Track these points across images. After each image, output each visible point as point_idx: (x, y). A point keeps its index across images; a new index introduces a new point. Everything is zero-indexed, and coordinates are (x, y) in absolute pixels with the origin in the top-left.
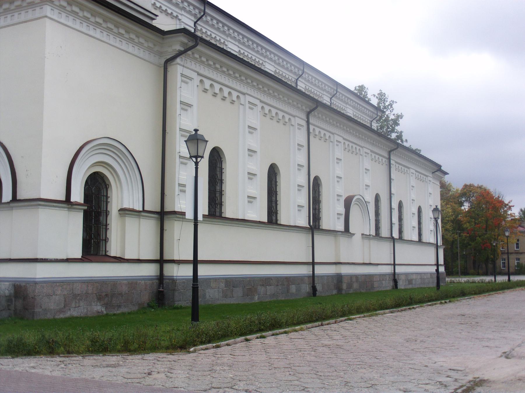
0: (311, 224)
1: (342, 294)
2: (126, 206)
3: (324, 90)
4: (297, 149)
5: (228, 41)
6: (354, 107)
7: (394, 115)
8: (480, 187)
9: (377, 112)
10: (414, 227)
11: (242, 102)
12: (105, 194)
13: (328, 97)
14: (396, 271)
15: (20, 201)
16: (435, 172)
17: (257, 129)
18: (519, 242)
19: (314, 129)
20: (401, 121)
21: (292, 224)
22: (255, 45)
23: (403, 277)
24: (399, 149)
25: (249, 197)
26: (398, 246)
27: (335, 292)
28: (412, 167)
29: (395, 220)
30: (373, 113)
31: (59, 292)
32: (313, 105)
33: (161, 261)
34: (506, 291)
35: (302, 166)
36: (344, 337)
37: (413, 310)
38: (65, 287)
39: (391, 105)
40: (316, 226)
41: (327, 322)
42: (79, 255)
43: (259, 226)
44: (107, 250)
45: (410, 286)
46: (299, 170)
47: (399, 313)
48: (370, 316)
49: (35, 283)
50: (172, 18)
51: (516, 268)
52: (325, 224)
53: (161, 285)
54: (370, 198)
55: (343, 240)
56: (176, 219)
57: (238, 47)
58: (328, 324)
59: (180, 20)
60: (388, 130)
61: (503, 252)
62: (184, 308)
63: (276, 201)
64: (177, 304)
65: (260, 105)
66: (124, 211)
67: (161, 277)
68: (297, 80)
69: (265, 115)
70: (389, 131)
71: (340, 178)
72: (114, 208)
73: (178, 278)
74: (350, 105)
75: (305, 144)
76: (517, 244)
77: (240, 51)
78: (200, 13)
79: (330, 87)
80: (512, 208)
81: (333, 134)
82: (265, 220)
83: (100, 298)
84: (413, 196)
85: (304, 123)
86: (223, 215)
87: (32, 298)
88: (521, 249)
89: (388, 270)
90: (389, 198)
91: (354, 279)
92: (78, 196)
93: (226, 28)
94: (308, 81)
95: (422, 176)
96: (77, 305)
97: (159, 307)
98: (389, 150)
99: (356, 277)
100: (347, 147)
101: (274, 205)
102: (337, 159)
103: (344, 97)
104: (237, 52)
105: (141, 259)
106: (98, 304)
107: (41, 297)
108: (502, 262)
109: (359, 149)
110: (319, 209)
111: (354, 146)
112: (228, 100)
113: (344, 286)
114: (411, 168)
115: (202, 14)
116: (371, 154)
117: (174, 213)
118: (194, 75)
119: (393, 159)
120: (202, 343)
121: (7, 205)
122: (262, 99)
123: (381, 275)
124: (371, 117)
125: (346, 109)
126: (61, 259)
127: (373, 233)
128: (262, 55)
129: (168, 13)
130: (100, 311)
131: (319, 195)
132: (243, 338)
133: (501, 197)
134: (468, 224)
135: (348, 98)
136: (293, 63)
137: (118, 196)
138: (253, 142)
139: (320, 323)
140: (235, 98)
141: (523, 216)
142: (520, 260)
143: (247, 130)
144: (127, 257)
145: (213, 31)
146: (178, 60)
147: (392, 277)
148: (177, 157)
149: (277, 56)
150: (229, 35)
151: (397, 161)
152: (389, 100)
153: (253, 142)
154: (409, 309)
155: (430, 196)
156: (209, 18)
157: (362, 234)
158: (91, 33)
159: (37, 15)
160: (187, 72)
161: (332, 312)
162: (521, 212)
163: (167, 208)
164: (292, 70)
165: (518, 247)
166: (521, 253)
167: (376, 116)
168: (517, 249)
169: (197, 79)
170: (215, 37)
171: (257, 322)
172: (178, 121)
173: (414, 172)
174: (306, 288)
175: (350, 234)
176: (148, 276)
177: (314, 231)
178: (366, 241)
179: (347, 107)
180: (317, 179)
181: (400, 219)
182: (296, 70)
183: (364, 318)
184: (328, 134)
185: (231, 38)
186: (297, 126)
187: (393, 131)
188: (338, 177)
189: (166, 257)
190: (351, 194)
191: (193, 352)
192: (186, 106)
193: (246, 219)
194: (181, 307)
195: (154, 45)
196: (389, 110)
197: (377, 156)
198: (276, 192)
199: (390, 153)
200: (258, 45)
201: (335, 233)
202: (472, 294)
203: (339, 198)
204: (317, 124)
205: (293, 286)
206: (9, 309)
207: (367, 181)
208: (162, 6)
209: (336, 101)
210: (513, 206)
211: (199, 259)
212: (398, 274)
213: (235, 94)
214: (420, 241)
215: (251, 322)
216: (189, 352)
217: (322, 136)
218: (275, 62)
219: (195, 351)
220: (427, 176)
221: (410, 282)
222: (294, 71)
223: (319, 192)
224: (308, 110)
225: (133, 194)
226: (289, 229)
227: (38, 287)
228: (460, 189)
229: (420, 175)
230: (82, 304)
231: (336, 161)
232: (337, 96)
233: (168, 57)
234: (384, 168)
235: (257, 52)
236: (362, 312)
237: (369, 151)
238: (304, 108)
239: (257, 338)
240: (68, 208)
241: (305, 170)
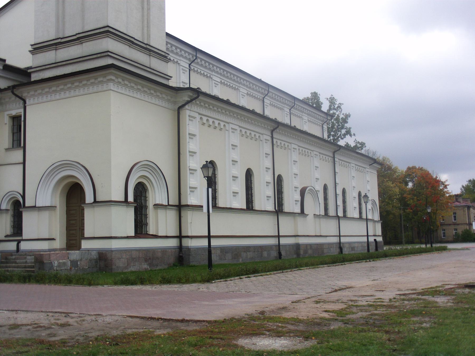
0: (277, 209)
1: (300, 257)
2: (157, 202)
3: (285, 104)
4: (265, 157)
5: (213, 75)
6: (308, 115)
7: (343, 114)
8: (421, 169)
10: (355, 208)
11: (227, 129)
12: (145, 196)
14: (281, 242)
15: (98, 202)
16: (372, 164)
17: (237, 146)
18: (456, 215)
19: (277, 142)
20: (349, 120)
21: (263, 210)
22: (232, 76)
23: (347, 246)
24: (341, 150)
25: (233, 192)
26: (343, 222)
27: (295, 256)
28: (352, 162)
29: (340, 202)
31: (124, 257)
32: (275, 126)
33: (180, 237)
34: (422, 254)
35: (269, 154)
36: (295, 277)
37: (344, 265)
38: (127, 253)
39: (339, 107)
40: (280, 210)
41: (285, 271)
42: (133, 234)
43: (240, 212)
44: (147, 230)
45: (353, 252)
46: (267, 171)
47: (334, 267)
48: (313, 268)
49: (111, 251)
50: (173, 63)
51: (454, 237)
52: (286, 208)
53: (181, 252)
54: (319, 188)
55: (300, 220)
56: (189, 210)
58: (286, 272)
59: (179, 64)
60: (339, 127)
61: (455, 223)
62: (196, 266)
63: (252, 194)
64: (191, 264)
65: (239, 129)
66: (157, 206)
67: (180, 247)
68: (264, 98)
69: (242, 136)
70: (339, 128)
71: (297, 175)
72: (150, 204)
73: (191, 247)
74: (305, 113)
75: (270, 152)
76: (455, 217)
77: (221, 81)
78: (193, 57)
79: (289, 101)
80: (448, 186)
81: (290, 143)
82: (245, 208)
83: (146, 261)
84: (354, 184)
85: (269, 138)
86: (217, 206)
87: (110, 260)
88: (458, 221)
89: (335, 240)
90: (334, 186)
91: (309, 247)
92: (131, 198)
93: (211, 66)
94: (272, 98)
95: (361, 168)
96: (134, 265)
97: (180, 266)
98: (334, 151)
99: (311, 246)
100: (301, 152)
101: (250, 197)
102: (294, 161)
103: (300, 108)
104: (219, 82)
105: (168, 236)
106: (145, 264)
107: (115, 259)
108: (442, 232)
109: (310, 153)
110: (282, 198)
111: (307, 150)
112: (218, 129)
113: (302, 252)
115: (195, 58)
116: (320, 155)
117: (188, 206)
118: (196, 115)
119: (337, 157)
120: (217, 279)
121: (91, 205)
122: (240, 125)
123: (329, 244)
124: (322, 121)
125: (302, 117)
126: (124, 237)
127: (323, 213)
128: (237, 82)
130: (146, 268)
131: (282, 188)
132: (239, 277)
133: (438, 177)
134: (411, 200)
135: (304, 108)
137: (153, 197)
138: (235, 155)
139: (281, 271)
140: (222, 127)
141: (464, 191)
142: (458, 230)
143: (231, 147)
144: (160, 234)
145: (202, 69)
146: (187, 107)
147: (338, 246)
148: (188, 170)
149: (249, 81)
150: (213, 71)
151: (340, 158)
152: (337, 103)
153: (235, 155)
154: (341, 265)
155: (368, 183)
156: (199, 60)
157: (314, 215)
158: (135, 95)
159: (105, 89)
160: (193, 114)
161: (289, 266)
162: (463, 189)
164: (259, 91)
165: (455, 219)
166: (458, 224)
167: (326, 120)
168: (455, 221)
169: (198, 117)
170: (204, 73)
171: (245, 269)
172: (188, 146)
174: (274, 254)
175: (304, 215)
176: (173, 246)
177: (279, 215)
178: (317, 220)
179: (303, 115)
180: (279, 177)
181: (344, 202)
182: (263, 90)
183: (310, 269)
184: (287, 144)
185: (215, 72)
186: (264, 141)
187: (343, 128)
188: (295, 174)
189: (183, 234)
190: (306, 186)
191: (214, 283)
192: (192, 135)
193: (232, 207)
194: (194, 265)
195: (171, 97)
196: (339, 111)
197: (324, 156)
198: (251, 187)
199: (334, 153)
200: (234, 75)
201: (294, 215)
202: (393, 256)
203: (296, 189)
204: (278, 138)
205: (265, 252)
206: (97, 267)
207: (317, 176)
209: (294, 111)
210: (448, 185)
212: (343, 243)
213: (222, 124)
214: (361, 218)
215: (242, 269)
216: (212, 283)
217: (283, 145)
218: (247, 86)
219: (215, 282)
220: (365, 168)
221: (353, 249)
223: (281, 186)
224: (272, 129)
225: (162, 194)
226: (261, 213)
227: (114, 253)
228: (404, 171)
229: (359, 167)
230: (136, 263)
231: (293, 162)
232: (295, 107)
233: (180, 105)
234: (330, 165)
235: (234, 80)
236: (309, 266)
237: (318, 154)
238: (269, 127)
239: (246, 278)
240: (127, 206)
241: (271, 171)
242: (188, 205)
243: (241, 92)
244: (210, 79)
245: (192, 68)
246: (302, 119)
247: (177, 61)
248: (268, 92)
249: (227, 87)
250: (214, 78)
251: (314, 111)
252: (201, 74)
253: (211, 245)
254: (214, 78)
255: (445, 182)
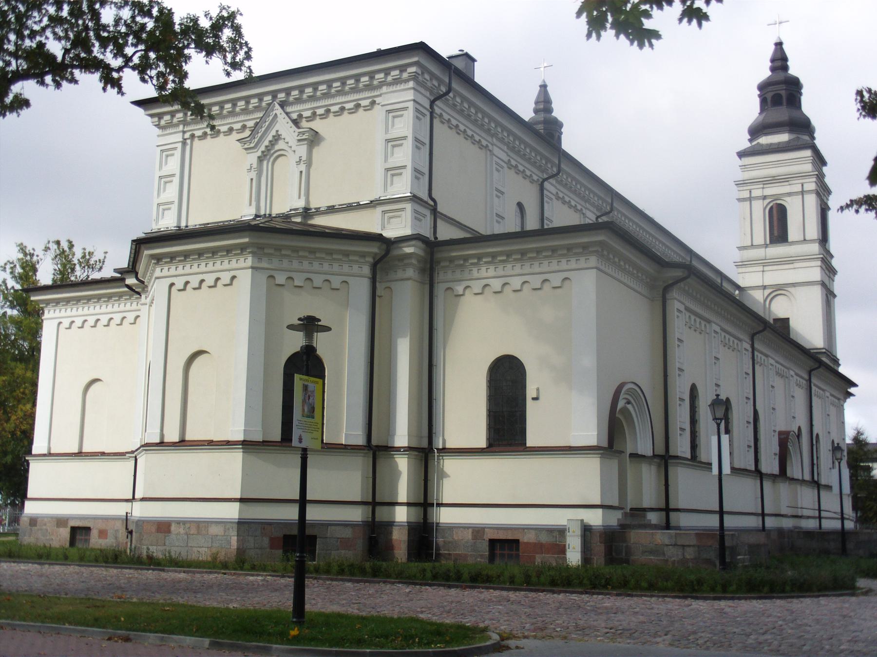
9: (559, 161)
13: (425, 96)
30: (604, 201)
31: (174, 536)
57: (508, 155)
59: (583, 214)
66: (634, 456)
77: (509, 161)
85: (749, 347)
104: (554, 195)
114: (770, 357)
115: (444, 89)
117: (677, 457)
129: (577, 210)
136: (649, 231)
163: (672, 453)
170: (570, 201)
173: (718, 329)
189: (672, 506)
208: (475, 135)
211: (308, 499)
222: (500, 136)
232: (448, 100)
242: (678, 456)
243: (494, 157)
244: (488, 152)
245: (437, 110)
246: (491, 155)
247: (581, 209)
248: (449, 90)
249: (449, 130)
250: (496, 151)
251: (643, 225)
252: (570, 206)
253: (307, 518)
254: (496, 151)
255: (211, 19)
